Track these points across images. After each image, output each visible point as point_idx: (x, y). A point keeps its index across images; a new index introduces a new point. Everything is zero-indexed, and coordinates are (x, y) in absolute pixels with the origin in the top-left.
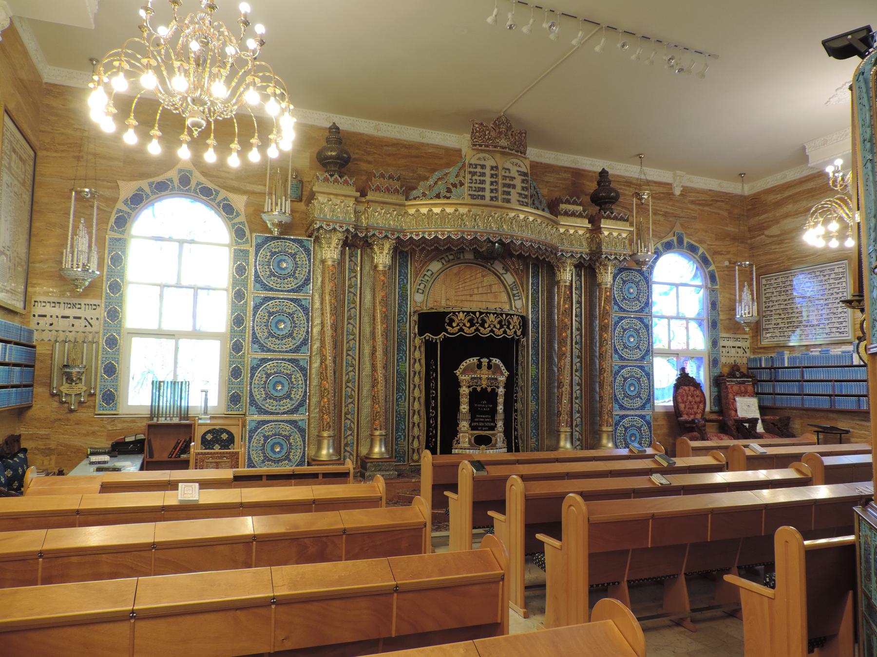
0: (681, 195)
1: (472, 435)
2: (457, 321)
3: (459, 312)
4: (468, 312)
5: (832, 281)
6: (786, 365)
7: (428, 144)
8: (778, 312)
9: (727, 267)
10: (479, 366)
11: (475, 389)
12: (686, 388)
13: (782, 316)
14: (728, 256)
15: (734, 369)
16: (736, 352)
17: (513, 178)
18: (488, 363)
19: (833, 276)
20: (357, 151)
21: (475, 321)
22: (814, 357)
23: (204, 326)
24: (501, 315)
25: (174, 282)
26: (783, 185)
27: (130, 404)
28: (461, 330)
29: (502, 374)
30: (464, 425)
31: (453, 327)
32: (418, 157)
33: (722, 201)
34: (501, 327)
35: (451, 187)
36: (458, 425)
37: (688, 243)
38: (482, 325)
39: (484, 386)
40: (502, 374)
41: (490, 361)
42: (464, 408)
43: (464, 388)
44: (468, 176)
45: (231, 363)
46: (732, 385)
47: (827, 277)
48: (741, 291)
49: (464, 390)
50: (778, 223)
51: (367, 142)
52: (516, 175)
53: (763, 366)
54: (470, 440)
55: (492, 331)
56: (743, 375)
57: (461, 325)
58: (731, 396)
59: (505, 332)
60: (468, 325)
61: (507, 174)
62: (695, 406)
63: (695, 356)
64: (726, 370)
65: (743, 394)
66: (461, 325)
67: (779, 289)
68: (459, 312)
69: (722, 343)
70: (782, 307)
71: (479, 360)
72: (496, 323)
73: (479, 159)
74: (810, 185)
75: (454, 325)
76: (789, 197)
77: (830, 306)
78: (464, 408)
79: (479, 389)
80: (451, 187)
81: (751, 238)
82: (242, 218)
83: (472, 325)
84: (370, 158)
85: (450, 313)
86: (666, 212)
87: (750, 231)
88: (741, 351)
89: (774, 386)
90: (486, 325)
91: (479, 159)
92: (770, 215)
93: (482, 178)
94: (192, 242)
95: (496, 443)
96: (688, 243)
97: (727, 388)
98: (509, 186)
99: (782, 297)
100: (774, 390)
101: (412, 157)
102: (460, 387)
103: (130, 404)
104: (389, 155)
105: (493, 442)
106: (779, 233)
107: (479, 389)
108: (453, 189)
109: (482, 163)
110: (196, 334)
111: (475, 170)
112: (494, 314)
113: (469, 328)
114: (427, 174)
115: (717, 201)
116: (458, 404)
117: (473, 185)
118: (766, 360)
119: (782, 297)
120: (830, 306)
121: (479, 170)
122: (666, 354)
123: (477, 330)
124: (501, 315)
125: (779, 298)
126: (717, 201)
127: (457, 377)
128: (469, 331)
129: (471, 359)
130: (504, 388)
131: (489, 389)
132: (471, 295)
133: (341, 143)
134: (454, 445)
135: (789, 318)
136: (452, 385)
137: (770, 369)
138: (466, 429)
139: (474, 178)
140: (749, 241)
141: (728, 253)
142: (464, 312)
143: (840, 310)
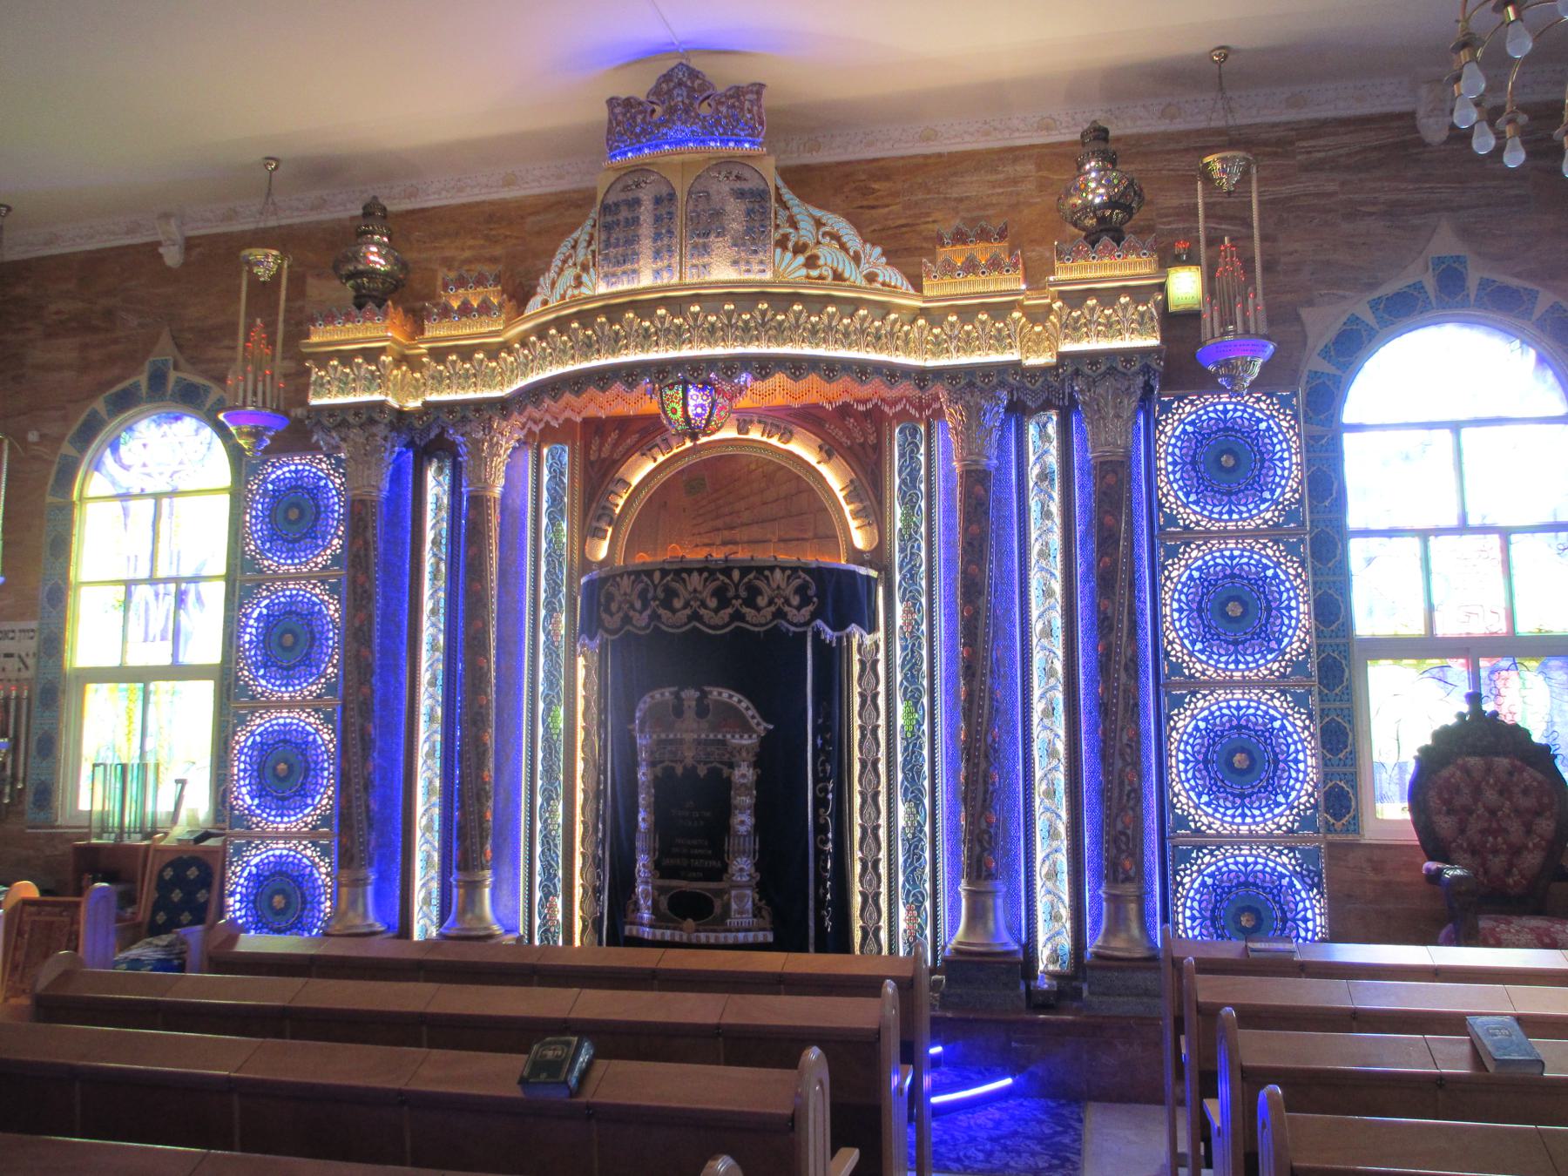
2: (618, 598)
3: (772, 569)
4: (795, 570)
10: (678, 711)
11: (669, 771)
18: (700, 701)
20: (471, 242)
21: (731, 593)
23: (189, 657)
25: (1453, 522)
31: (758, 609)
35: (808, 253)
38: (750, 602)
39: (689, 762)
40: (746, 728)
41: (704, 695)
42: (743, 821)
48: (250, 327)
55: (696, 616)
57: (695, 604)
60: (713, 603)
66: (780, 601)
71: (677, 695)
72: (789, 591)
75: (761, 601)
78: (743, 821)
79: (679, 770)
80: (808, 253)
90: (678, 604)
94: (173, 494)
105: (717, 910)
107: (679, 770)
108: (801, 259)
110: (178, 671)
112: (700, 571)
113: (716, 611)
122: (1425, 647)
123: (738, 616)
130: (755, 765)
133: (1106, 140)
142: (783, 569)
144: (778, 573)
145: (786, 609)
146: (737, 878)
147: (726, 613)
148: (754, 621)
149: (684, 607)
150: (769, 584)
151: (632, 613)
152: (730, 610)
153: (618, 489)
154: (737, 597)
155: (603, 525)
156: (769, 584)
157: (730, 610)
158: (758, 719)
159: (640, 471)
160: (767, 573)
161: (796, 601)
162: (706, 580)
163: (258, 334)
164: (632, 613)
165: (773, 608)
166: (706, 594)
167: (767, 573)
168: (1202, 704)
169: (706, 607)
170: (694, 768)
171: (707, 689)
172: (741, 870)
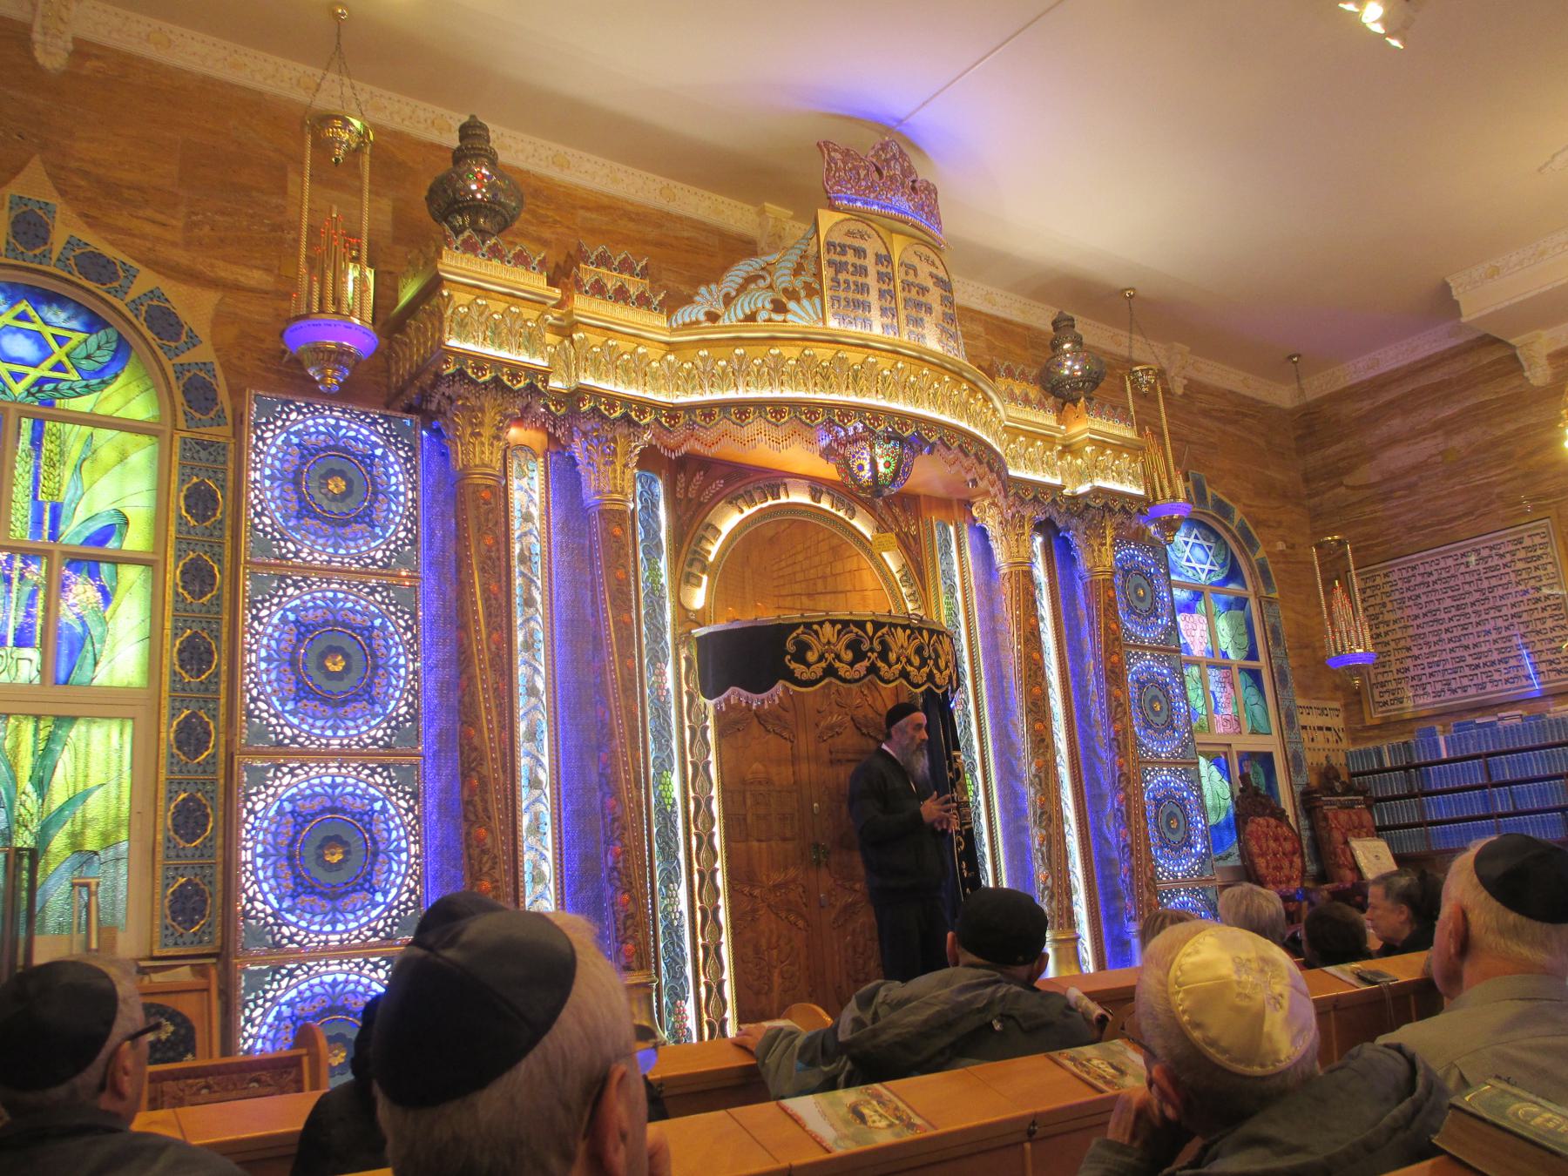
0: (1184, 395)
3: (821, 624)
5: (1520, 565)
6: (1444, 756)
8: (1402, 643)
12: (1261, 820)
13: (1416, 652)
14: (1280, 532)
15: (1328, 775)
16: (1325, 738)
17: (924, 290)
19: (1522, 554)
21: (865, 647)
22: (1511, 731)
24: (920, 630)
26: (1371, 381)
31: (808, 665)
33: (1254, 417)
34: (924, 663)
37: (1213, 496)
38: (883, 656)
45: (174, 785)
46: (1329, 806)
47: (1508, 558)
48: (1329, 593)
50: (1373, 458)
51: (536, 193)
52: (930, 283)
53: (1388, 764)
56: (1348, 789)
58: (1337, 836)
59: (930, 676)
60: (848, 656)
61: (911, 278)
62: (1286, 864)
64: (1314, 781)
65: (1360, 830)
67: (1397, 596)
68: (821, 624)
69: (1302, 719)
70: (1411, 631)
72: (910, 651)
73: (849, 234)
75: (812, 657)
77: (1525, 617)
81: (1310, 496)
82: (204, 353)
83: (859, 656)
84: (547, 234)
85: (796, 626)
87: (1307, 481)
88: (1331, 736)
89: (1421, 808)
91: (849, 234)
93: (860, 280)
96: (1213, 496)
97: (1326, 818)
99: (1408, 612)
100: (1423, 815)
104: (592, 231)
106: (1378, 478)
108: (792, 305)
109: (857, 243)
111: (844, 259)
112: (904, 627)
113: (852, 664)
114: (686, 290)
115: (1246, 415)
118: (1394, 750)
119: (1408, 612)
120: (1525, 617)
121: (850, 257)
124: (920, 630)
125: (1399, 614)
126: (1246, 415)
132: (810, 595)
135: (1433, 654)
137: (1406, 769)
139: (842, 277)
141: (1280, 524)
142: (833, 623)
143: (1550, 623)
144: (827, 626)
145: (837, 664)
151: (909, 668)
152: (866, 663)
153: (709, 535)
154: (872, 650)
155: (695, 570)
157: (866, 663)
159: (730, 521)
160: (815, 627)
162: (839, 632)
164: (909, 668)
165: (823, 664)
167: (815, 627)
168: (290, 784)
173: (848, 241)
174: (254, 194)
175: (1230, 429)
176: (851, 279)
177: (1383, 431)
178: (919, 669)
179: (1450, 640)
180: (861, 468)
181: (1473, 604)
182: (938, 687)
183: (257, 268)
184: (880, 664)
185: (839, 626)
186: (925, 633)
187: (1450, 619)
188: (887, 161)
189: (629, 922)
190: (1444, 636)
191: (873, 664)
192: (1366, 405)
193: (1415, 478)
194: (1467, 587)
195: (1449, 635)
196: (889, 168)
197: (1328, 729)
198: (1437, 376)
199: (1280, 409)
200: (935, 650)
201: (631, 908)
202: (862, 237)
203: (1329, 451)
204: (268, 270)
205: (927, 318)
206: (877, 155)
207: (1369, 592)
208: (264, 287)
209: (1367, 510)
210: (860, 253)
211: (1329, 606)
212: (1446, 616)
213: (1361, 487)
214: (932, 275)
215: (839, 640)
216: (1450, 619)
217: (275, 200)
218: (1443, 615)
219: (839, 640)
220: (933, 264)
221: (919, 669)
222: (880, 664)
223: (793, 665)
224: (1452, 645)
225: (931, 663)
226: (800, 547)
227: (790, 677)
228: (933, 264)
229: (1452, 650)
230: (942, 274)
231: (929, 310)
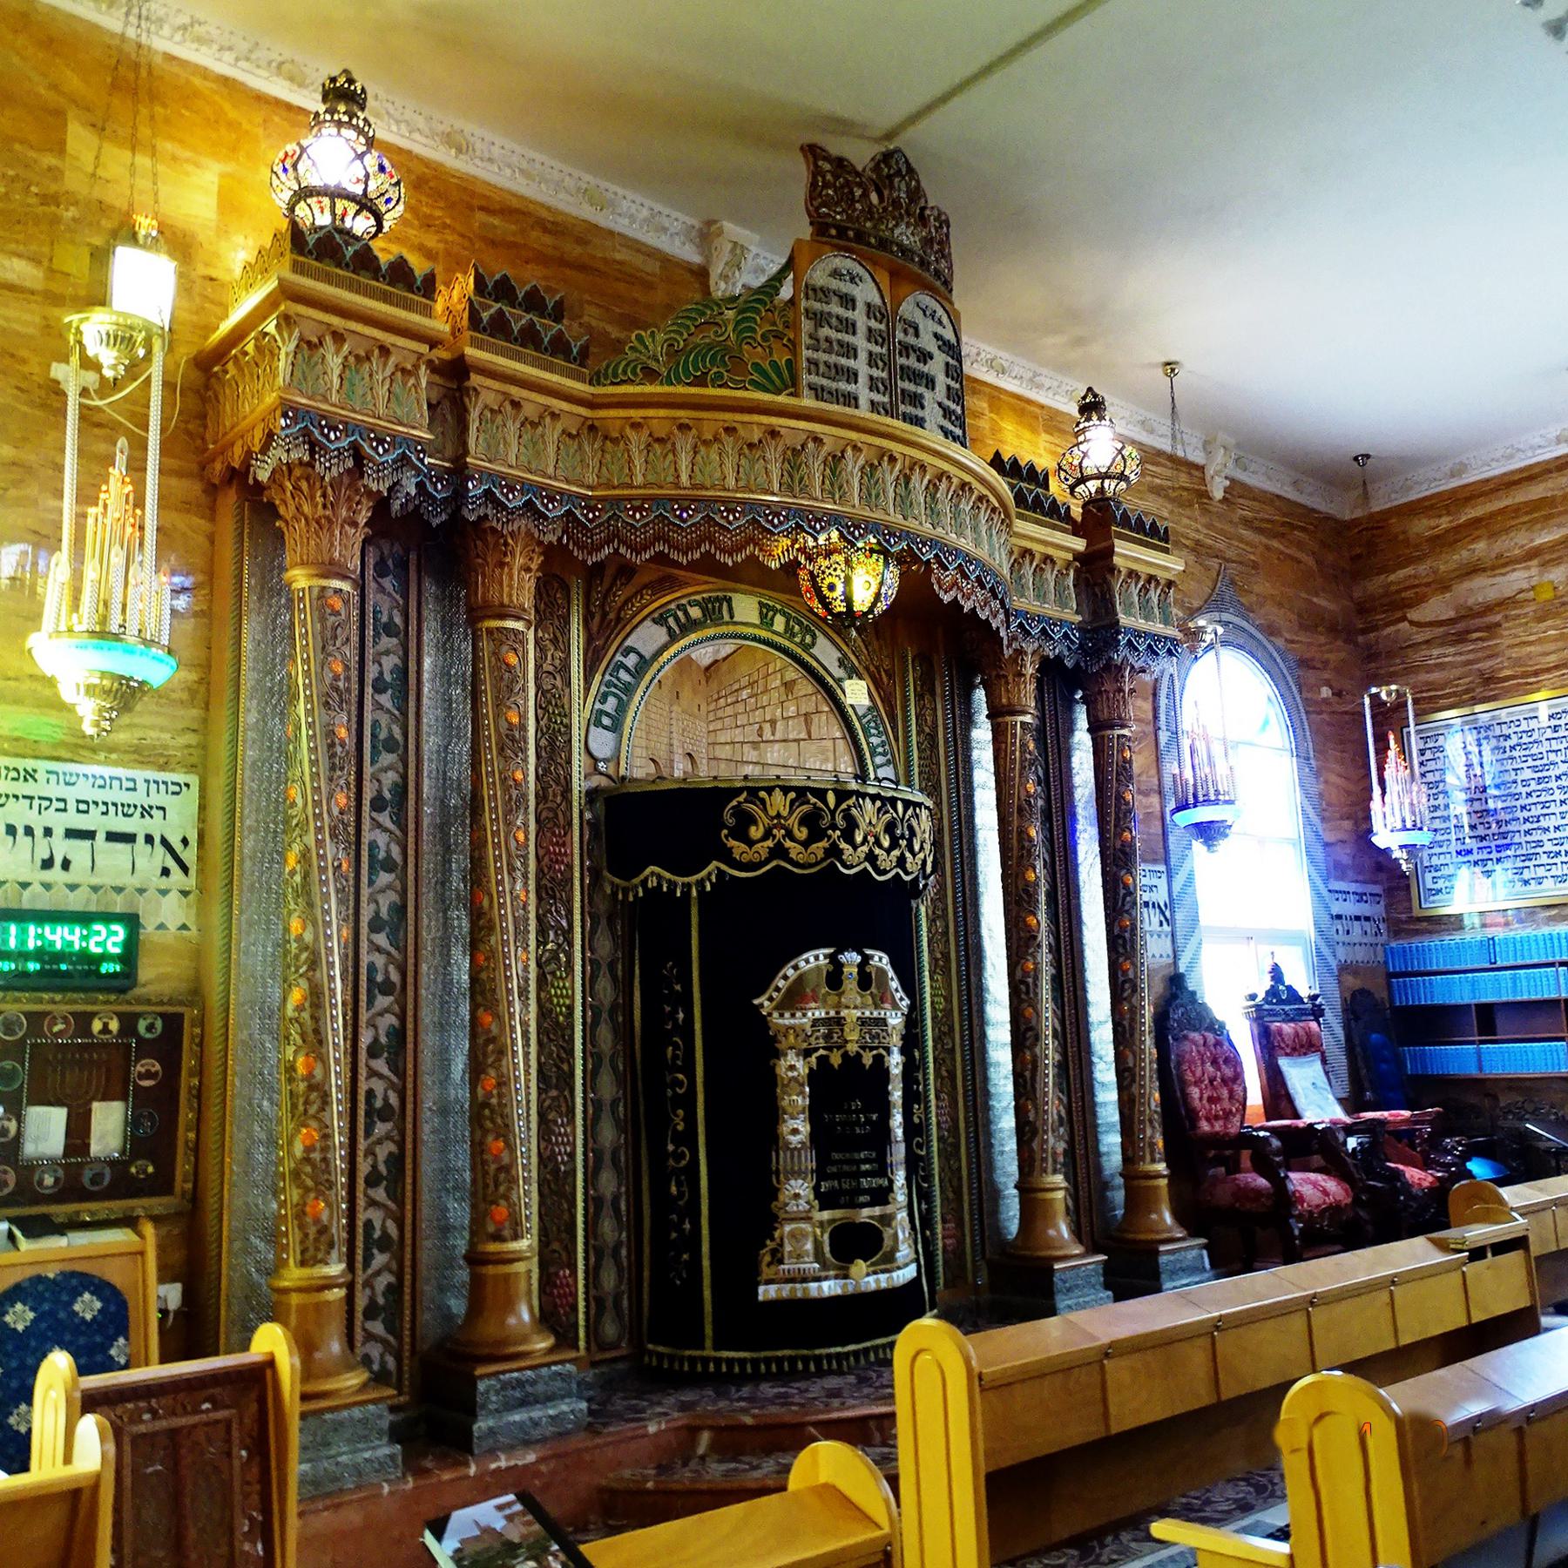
0: (1224, 500)
1: (821, 1224)
2: (764, 821)
3: (770, 790)
4: (801, 792)
7: (611, 233)
9: (1324, 700)
10: (835, 978)
11: (823, 1060)
14: (1326, 676)
17: (925, 357)
27: (96, 1105)
28: (779, 852)
29: (895, 1006)
30: (798, 1190)
31: (751, 843)
32: (582, 268)
33: (1303, 529)
34: (894, 844)
36: (774, 1193)
38: (848, 836)
39: (852, 1048)
41: (866, 959)
42: (797, 1128)
43: (792, 1058)
44: (806, 325)
48: (1382, 750)
49: (794, 1066)
52: (931, 345)
54: (818, 1245)
59: (901, 861)
60: (802, 834)
61: (911, 340)
63: (1290, 938)
66: (779, 833)
68: (770, 790)
71: (833, 958)
72: (880, 828)
73: (836, 274)
74: (1536, 491)
75: (755, 832)
76: (1476, 522)
78: (797, 1128)
79: (836, 1059)
81: (1364, 632)
83: (816, 834)
85: (739, 791)
86: (1198, 542)
92: (1423, 569)
95: (895, 1249)
98: (916, 376)
101: (563, 262)
102: (778, 1054)
103: (96, 1105)
105: (887, 1243)
106: (1452, 614)
107: (836, 1059)
109: (846, 287)
111: (826, 308)
113: (806, 844)
116: (772, 1114)
117: (822, 356)
121: (836, 308)
127: (763, 1022)
128: (803, 855)
129: (810, 955)
131: (868, 1059)
134: (767, 1272)
136: (747, 1052)
138: (803, 1206)
140: (1360, 639)
142: (786, 790)
144: (778, 793)
145: (788, 844)
146: (792, 1207)
147: (820, 847)
148: (801, 859)
149: (764, 839)
150: (765, 810)
151: (877, 851)
152: (824, 844)
154: (834, 827)
156: (765, 810)
157: (824, 844)
158: (770, 992)
160: (763, 794)
161: (802, 834)
162: (792, 802)
163: (116, 487)
164: (877, 851)
165: (770, 843)
166: (793, 822)
167: (763, 794)
169: (793, 839)
170: (859, 1056)
171: (868, 952)
172: (797, 1196)
173: (835, 284)
174: (17, 146)
175: (1275, 544)
176: (834, 335)
177: (1462, 555)
178: (888, 851)
179: (1526, 820)
180: (832, 587)
181: (1558, 778)
182: (907, 873)
183: (19, 256)
184: (843, 845)
185: (792, 795)
186: (900, 806)
187: (1529, 794)
188: (889, 177)
189: (502, 1176)
190: (1519, 814)
191: (834, 846)
192: (1445, 522)
193: (1498, 618)
194: (1552, 756)
195: (1526, 814)
196: (892, 187)
197: (1367, 919)
198: (1536, 491)
199: (1336, 521)
200: (910, 828)
201: (506, 1160)
202: (852, 280)
203: (1392, 578)
204: (35, 260)
205: (927, 394)
206: (876, 169)
207: (1428, 755)
208: (28, 284)
209: (1435, 652)
210: (848, 301)
211: (1381, 769)
212: (1524, 790)
213: (1431, 624)
214: (936, 336)
215: (791, 812)
216: (1529, 794)
217: (49, 160)
218: (1520, 789)
219: (791, 812)
220: (940, 323)
221: (888, 851)
222: (843, 845)
223: (732, 843)
224: (1528, 826)
225: (903, 843)
226: (744, 681)
227: (726, 856)
228: (940, 323)
229: (1527, 832)
230: (948, 334)
231: (930, 383)
